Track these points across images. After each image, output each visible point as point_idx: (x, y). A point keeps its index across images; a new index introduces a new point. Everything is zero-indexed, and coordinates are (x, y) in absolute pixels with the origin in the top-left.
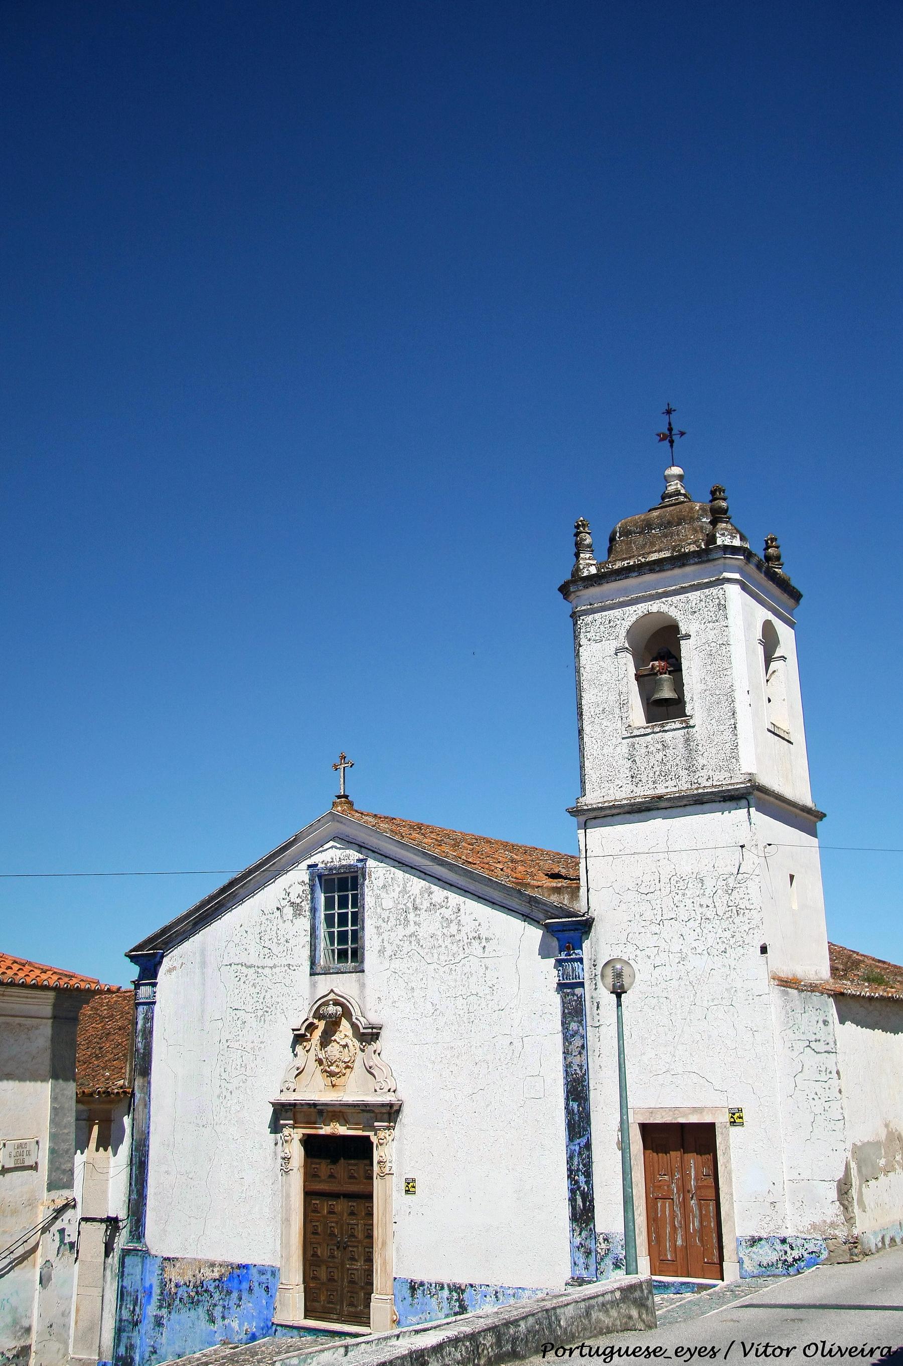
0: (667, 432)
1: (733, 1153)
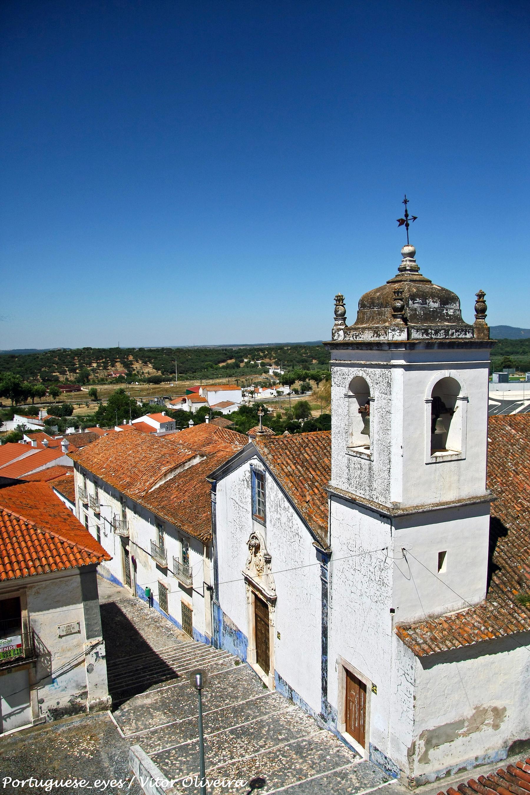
0: (404, 218)
1: (372, 704)
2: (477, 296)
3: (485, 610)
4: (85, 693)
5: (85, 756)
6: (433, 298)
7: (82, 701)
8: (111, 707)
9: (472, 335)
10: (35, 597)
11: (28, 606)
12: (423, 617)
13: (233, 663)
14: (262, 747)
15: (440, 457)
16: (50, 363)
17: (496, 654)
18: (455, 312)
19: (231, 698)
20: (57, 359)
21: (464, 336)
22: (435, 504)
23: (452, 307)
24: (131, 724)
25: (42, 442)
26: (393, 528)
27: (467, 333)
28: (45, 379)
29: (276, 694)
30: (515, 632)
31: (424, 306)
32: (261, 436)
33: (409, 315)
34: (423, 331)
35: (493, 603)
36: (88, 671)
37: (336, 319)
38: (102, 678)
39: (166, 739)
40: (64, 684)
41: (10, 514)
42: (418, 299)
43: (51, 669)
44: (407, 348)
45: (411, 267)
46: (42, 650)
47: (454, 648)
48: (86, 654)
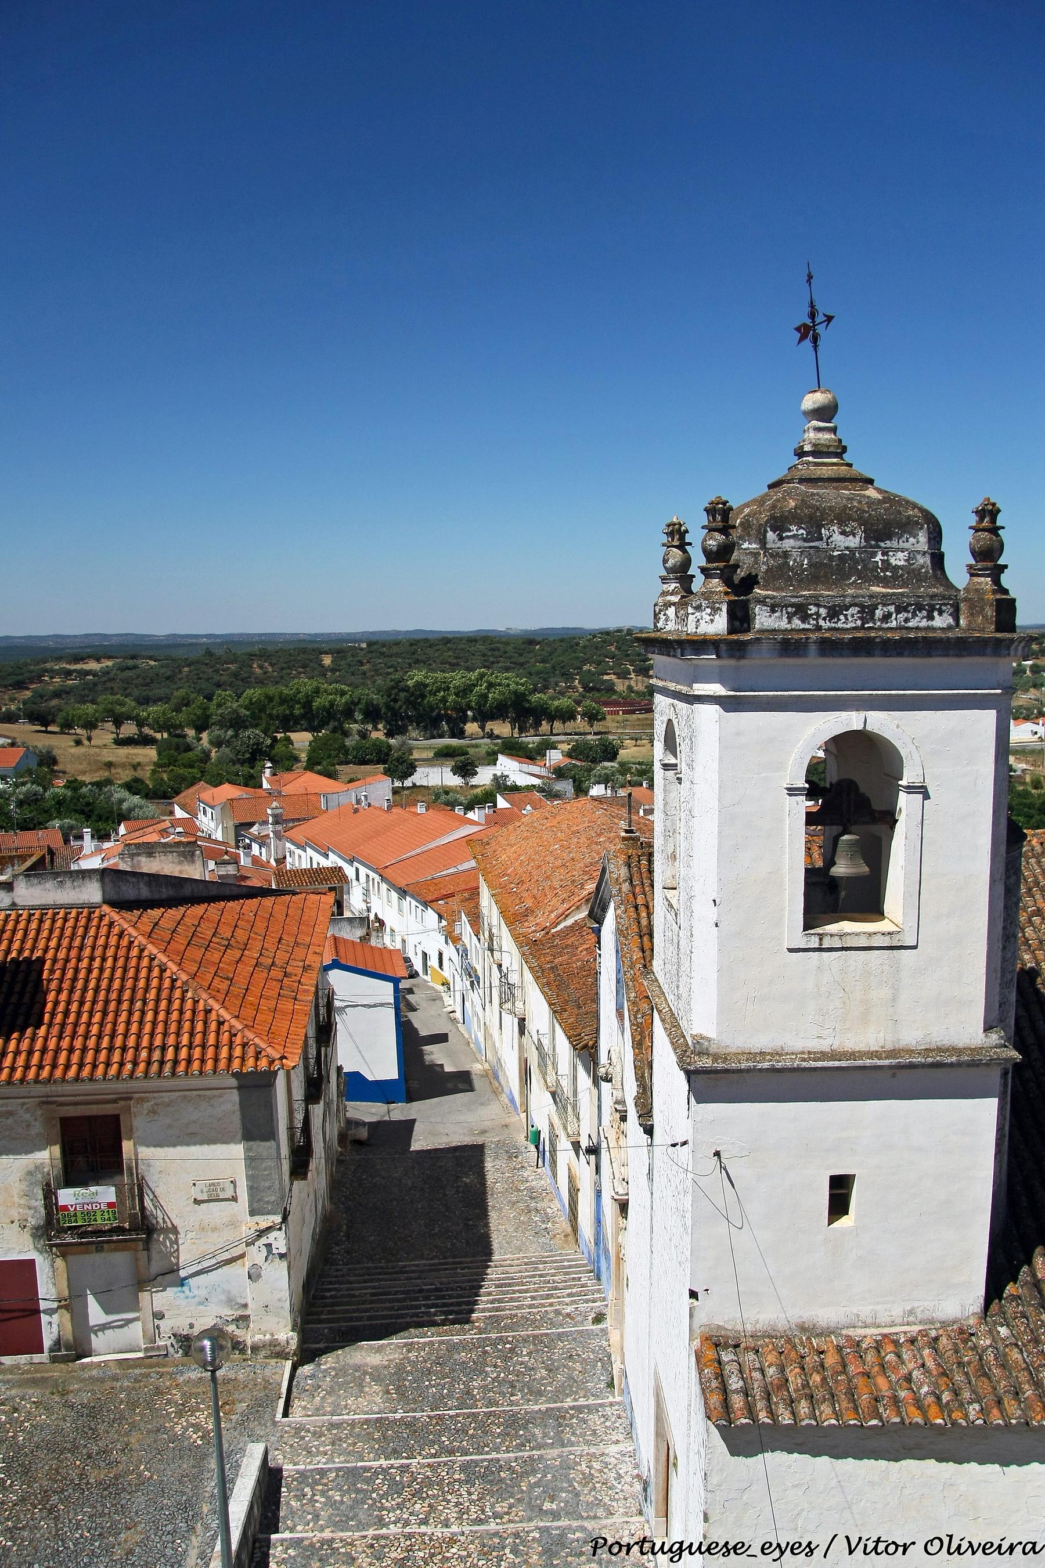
2: (976, 512)
3: (965, 1341)
4: (245, 1318)
5: (191, 1437)
6: (841, 523)
7: (237, 1332)
8: (294, 1354)
9: (951, 620)
10: (149, 1120)
11: (135, 1135)
12: (782, 1325)
13: (590, 1318)
14: (496, 1516)
15: (831, 935)
16: (600, 655)
17: (960, 1463)
18: (914, 558)
19: (531, 1392)
20: (613, 649)
21: (924, 623)
22: (815, 1053)
23: (902, 545)
24: (314, 1397)
25: (523, 812)
26: (692, 1099)
27: (936, 614)
28: (587, 686)
29: (617, 1407)
30: (1014, 1421)
31: (813, 544)
32: (624, 839)
33: (764, 568)
34: (789, 609)
35: (999, 1328)
36: (250, 1277)
37: (664, 580)
38: (279, 1296)
39: (345, 1445)
40: (203, 1293)
41: (155, 955)
42: (794, 528)
43: (178, 1258)
44: (723, 653)
45: (814, 445)
46: (161, 1221)
47: (814, 1423)
48: (248, 1245)
